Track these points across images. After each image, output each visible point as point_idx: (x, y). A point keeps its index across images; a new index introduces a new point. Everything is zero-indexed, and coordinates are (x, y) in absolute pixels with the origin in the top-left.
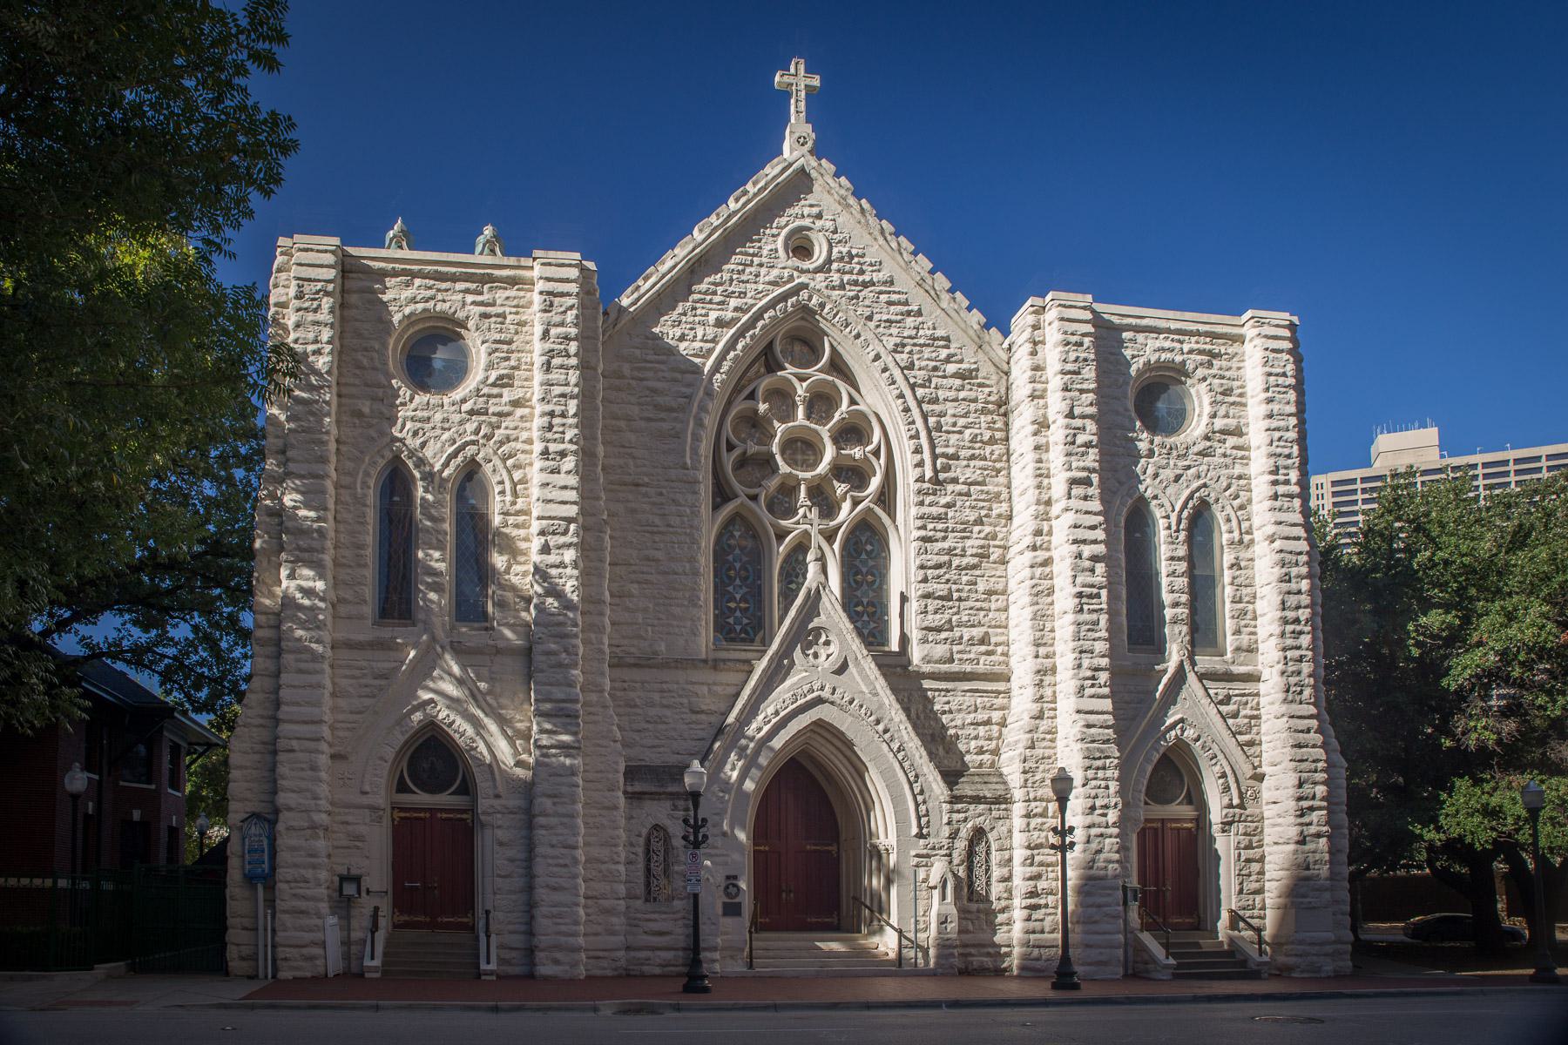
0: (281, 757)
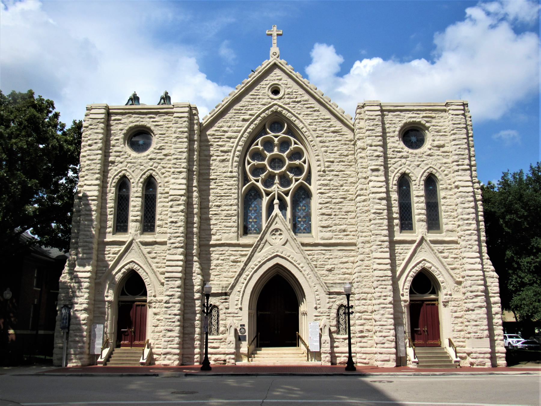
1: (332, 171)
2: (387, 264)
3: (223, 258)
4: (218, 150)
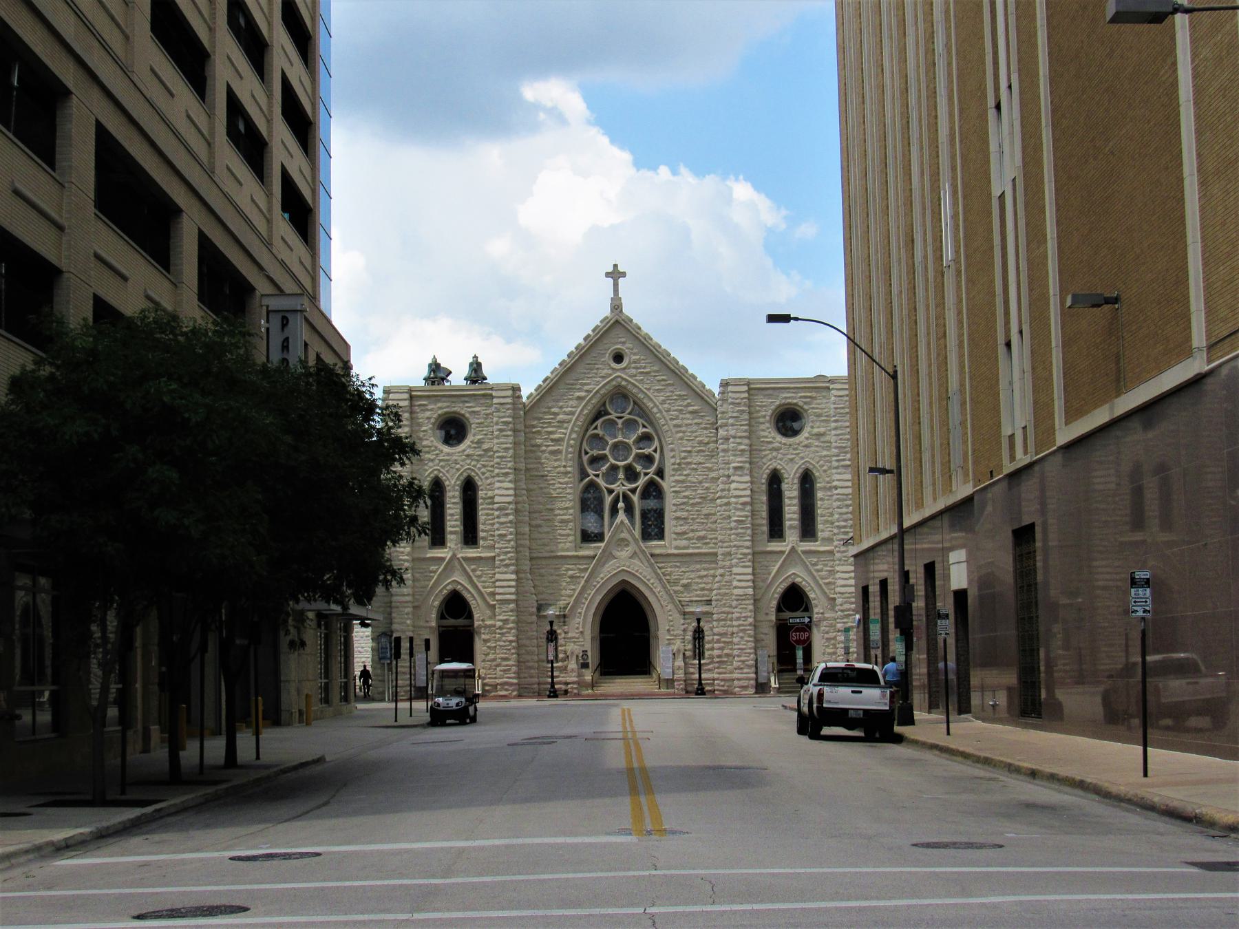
0: (394, 610)
1: (690, 463)
2: (748, 581)
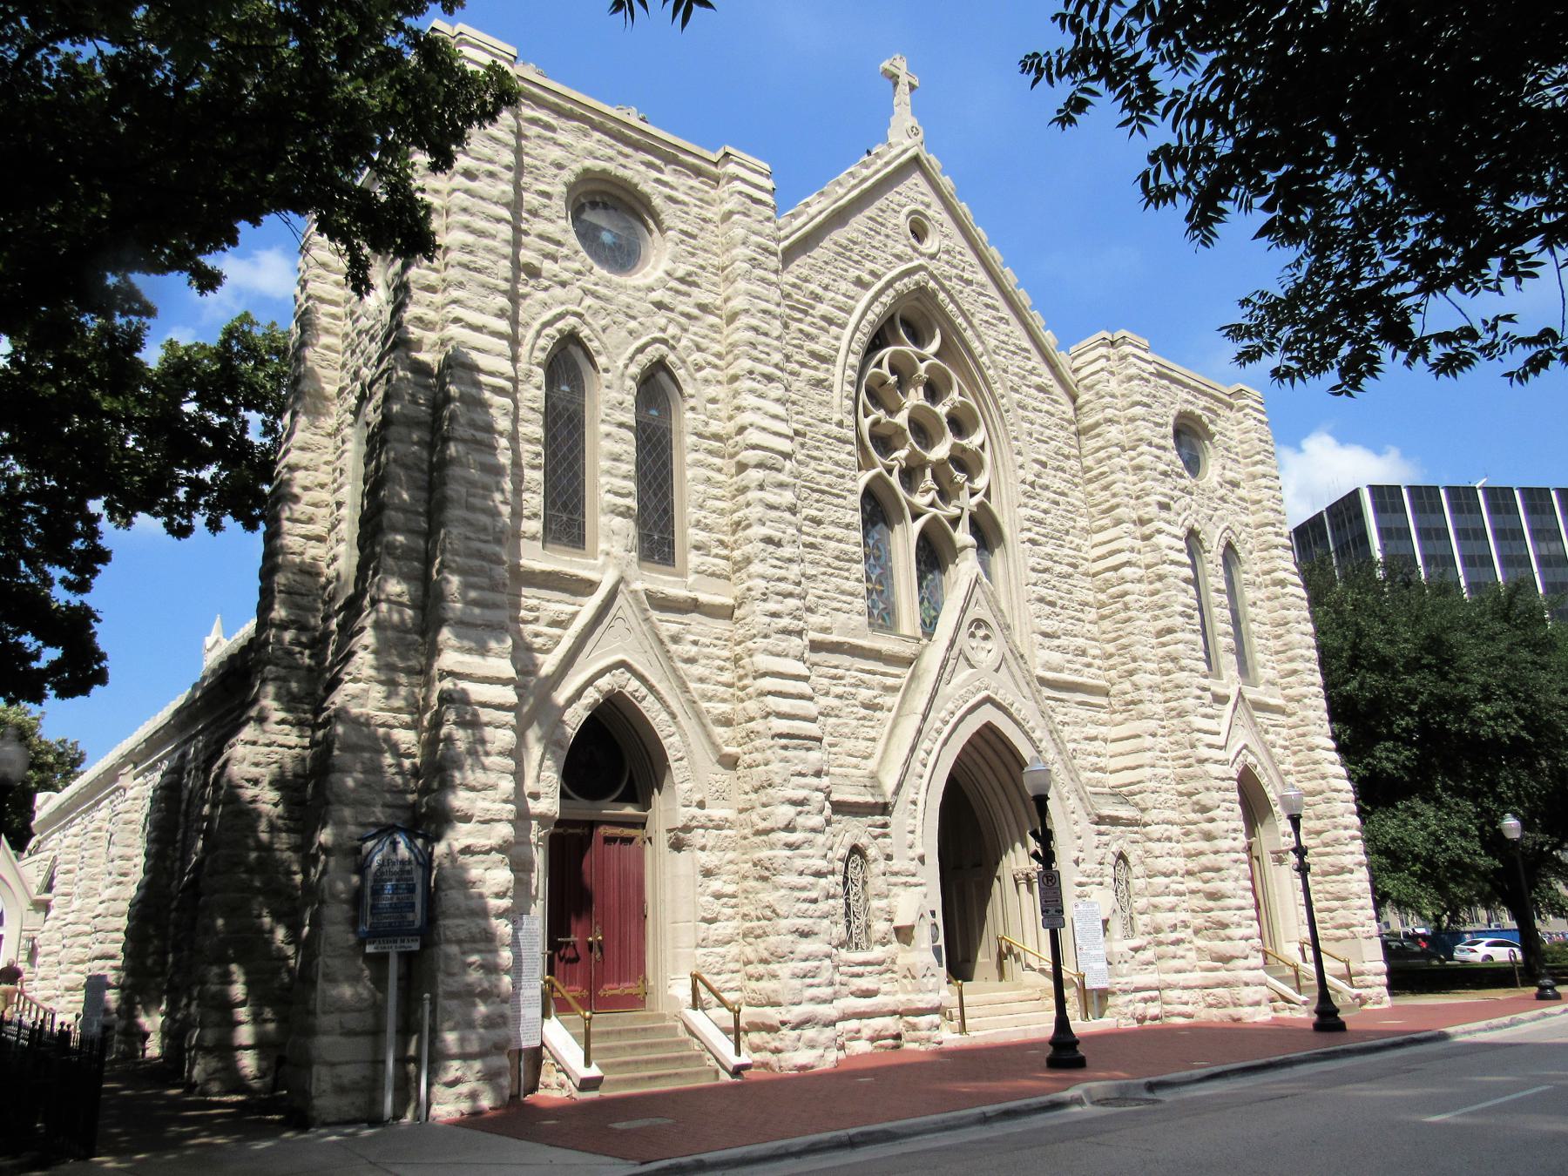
3: (839, 690)
4: (801, 347)
